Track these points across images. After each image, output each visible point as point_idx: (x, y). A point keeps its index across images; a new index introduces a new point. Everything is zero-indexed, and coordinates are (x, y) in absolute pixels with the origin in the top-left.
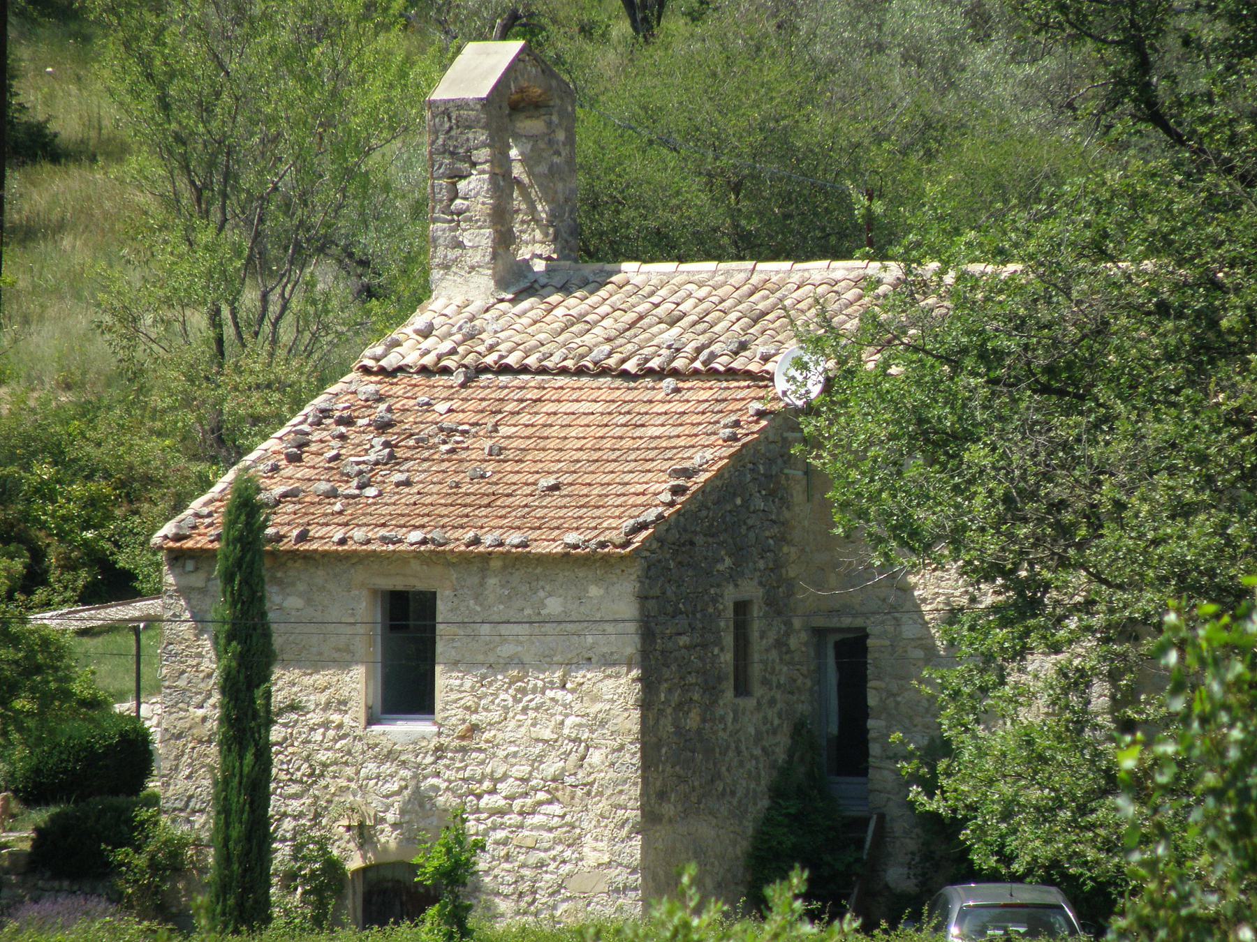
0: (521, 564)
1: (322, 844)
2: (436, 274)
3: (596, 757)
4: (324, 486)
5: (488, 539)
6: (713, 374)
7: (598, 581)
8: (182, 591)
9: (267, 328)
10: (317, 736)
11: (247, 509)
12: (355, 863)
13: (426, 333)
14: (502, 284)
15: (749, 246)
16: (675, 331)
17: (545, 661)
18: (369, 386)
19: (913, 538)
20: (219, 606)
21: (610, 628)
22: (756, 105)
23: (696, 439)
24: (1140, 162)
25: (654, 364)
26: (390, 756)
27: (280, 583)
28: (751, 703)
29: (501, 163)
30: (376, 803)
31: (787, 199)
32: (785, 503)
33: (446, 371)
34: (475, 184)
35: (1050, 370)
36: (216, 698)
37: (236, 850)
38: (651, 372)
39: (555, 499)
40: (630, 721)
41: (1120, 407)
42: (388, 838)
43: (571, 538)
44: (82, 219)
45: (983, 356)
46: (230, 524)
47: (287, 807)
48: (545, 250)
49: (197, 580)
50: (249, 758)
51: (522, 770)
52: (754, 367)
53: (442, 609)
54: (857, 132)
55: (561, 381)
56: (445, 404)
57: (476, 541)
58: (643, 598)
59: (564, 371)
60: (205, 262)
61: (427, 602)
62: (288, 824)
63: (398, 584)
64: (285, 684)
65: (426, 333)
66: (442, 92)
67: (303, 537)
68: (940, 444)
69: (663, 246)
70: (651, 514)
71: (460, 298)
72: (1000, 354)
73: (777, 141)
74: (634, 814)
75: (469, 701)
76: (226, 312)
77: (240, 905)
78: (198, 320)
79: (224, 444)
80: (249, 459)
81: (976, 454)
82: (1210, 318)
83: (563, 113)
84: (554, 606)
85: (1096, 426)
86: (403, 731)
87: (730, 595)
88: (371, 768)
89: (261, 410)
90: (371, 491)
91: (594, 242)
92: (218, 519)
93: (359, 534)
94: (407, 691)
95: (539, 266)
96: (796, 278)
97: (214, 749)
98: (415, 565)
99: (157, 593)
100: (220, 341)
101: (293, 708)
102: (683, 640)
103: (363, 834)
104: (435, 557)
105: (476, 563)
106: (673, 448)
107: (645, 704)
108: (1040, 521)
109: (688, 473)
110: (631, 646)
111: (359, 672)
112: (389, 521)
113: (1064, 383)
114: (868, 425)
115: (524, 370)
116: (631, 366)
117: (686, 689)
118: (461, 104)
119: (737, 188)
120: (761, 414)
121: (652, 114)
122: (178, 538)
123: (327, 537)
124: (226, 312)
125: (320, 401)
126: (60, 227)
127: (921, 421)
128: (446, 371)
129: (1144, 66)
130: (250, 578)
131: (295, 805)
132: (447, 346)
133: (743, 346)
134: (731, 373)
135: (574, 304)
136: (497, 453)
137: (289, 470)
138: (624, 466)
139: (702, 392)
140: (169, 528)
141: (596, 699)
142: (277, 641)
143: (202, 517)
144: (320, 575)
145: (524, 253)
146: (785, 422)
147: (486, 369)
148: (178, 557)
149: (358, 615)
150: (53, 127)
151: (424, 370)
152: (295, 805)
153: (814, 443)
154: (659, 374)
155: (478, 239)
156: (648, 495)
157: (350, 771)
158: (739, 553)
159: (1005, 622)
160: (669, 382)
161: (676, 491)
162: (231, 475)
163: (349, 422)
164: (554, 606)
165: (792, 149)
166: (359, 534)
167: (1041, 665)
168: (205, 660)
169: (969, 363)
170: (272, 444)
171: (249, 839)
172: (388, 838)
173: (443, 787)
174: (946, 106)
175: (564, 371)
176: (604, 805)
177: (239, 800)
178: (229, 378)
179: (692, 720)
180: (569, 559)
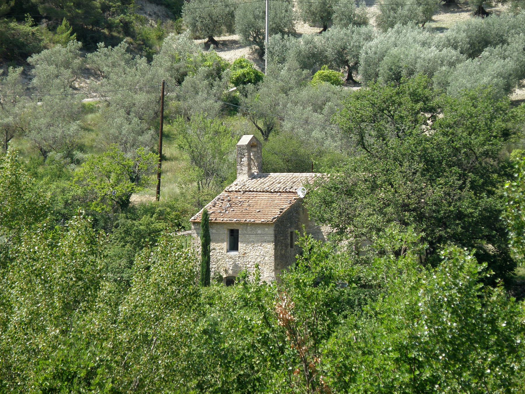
0: (253, 224)
1: (219, 273)
2: (238, 175)
3: (266, 258)
4: (219, 211)
5: (248, 220)
6: (287, 192)
7: (267, 228)
8: (195, 229)
9: (207, 185)
10: (218, 254)
11: (206, 214)
12: (225, 276)
13: (236, 185)
14: (249, 177)
15: (289, 171)
16: (280, 185)
17: (258, 241)
18: (226, 194)
19: (323, 220)
20: (201, 231)
21: (269, 235)
22: (292, 147)
23: (284, 203)
24: (362, 155)
25: (276, 190)
26: (231, 258)
27: (212, 228)
28: (293, 249)
29: (249, 155)
30: (228, 266)
31: (297, 163)
32: (299, 214)
33: (240, 191)
34: (245, 159)
35: (347, 191)
36: (201, 247)
37: (204, 273)
38: (276, 192)
39: (259, 213)
40: (272, 252)
41: (359, 197)
42: (230, 272)
43: (263, 220)
44: (171, 170)
45: (335, 188)
46: (203, 217)
47: (213, 266)
48: (257, 171)
49: (197, 227)
50: (206, 258)
51: (254, 260)
52: (294, 191)
53: (240, 232)
54: (309, 152)
55: (260, 193)
56: (240, 197)
57: (246, 221)
58: (275, 231)
59: (260, 192)
60: (197, 173)
61: (237, 231)
62: (213, 269)
63: (232, 228)
64: (212, 245)
65: (236, 185)
66: (240, 143)
67: (216, 220)
68: (328, 204)
69: (275, 171)
70: (276, 216)
71: (242, 178)
72: (338, 188)
73: (295, 153)
74: (273, 268)
75: (244, 248)
76: (200, 182)
77: (205, 283)
78: (195, 184)
79: (200, 205)
80: (205, 207)
81: (334, 205)
82: (374, 182)
83: (260, 147)
84: (259, 232)
85: (355, 200)
86: (233, 253)
87: (290, 230)
88: (227, 260)
89: (207, 199)
90: (227, 212)
91: (265, 170)
92: (201, 216)
93: (225, 219)
94: (234, 246)
95: (256, 174)
96: (301, 176)
97: (200, 256)
98: (235, 225)
99: (190, 229)
100: (199, 187)
101: (214, 249)
102: (282, 238)
103: (226, 271)
104: (239, 223)
105: (246, 224)
106: (280, 205)
107: (275, 249)
108: (346, 216)
109: (282, 209)
110: (273, 239)
111: (225, 243)
112: (231, 217)
113: (349, 193)
114: (316, 200)
115: (254, 191)
116: (272, 191)
117: (282, 246)
118: (243, 146)
119: (288, 162)
120: (295, 199)
121: (274, 149)
122: (194, 220)
123: (220, 220)
124: (200, 182)
125: (218, 197)
126: (167, 171)
127: (325, 199)
128: (240, 191)
129: (362, 139)
130: (206, 227)
131: (214, 266)
132: (240, 187)
133: (292, 187)
134: (290, 192)
135: (262, 180)
136: (249, 205)
137: (213, 208)
138: (273, 208)
139: (284, 195)
140: (193, 218)
141: (266, 248)
142: (211, 238)
143: (198, 216)
144: (219, 226)
145: (253, 171)
146: (300, 200)
147: (247, 191)
148: (194, 223)
149: (225, 234)
150: (165, 155)
151: (236, 191)
152: (214, 266)
153: (306, 203)
154: (277, 192)
155: (245, 169)
156: (276, 213)
157: (224, 260)
158: (291, 223)
159: (338, 234)
160: (279, 193)
161: (281, 212)
162: (203, 209)
163: (223, 200)
164: (259, 232)
165: (298, 155)
166: (225, 219)
167: (345, 243)
168: (198, 241)
169: (333, 189)
170: (210, 204)
171: (206, 271)
172: (230, 272)
173: (240, 262)
174: (323, 148)
175: (260, 192)
176: (268, 266)
177: (205, 265)
178: (201, 193)
179: (283, 252)
180: (262, 224)
